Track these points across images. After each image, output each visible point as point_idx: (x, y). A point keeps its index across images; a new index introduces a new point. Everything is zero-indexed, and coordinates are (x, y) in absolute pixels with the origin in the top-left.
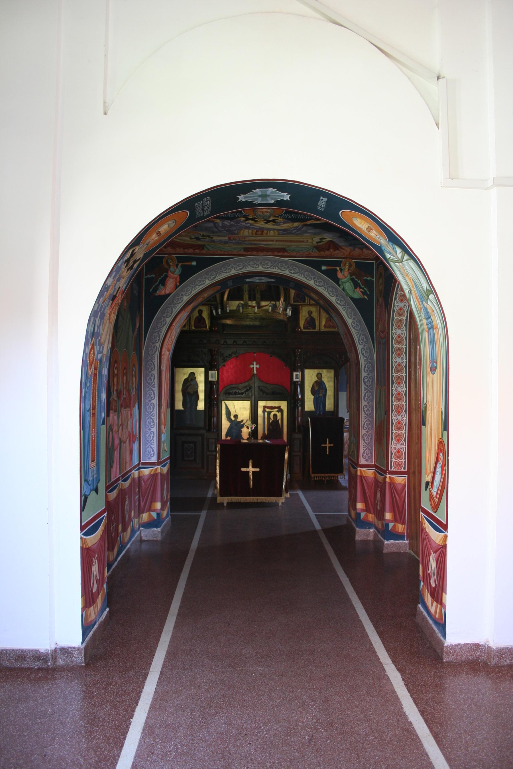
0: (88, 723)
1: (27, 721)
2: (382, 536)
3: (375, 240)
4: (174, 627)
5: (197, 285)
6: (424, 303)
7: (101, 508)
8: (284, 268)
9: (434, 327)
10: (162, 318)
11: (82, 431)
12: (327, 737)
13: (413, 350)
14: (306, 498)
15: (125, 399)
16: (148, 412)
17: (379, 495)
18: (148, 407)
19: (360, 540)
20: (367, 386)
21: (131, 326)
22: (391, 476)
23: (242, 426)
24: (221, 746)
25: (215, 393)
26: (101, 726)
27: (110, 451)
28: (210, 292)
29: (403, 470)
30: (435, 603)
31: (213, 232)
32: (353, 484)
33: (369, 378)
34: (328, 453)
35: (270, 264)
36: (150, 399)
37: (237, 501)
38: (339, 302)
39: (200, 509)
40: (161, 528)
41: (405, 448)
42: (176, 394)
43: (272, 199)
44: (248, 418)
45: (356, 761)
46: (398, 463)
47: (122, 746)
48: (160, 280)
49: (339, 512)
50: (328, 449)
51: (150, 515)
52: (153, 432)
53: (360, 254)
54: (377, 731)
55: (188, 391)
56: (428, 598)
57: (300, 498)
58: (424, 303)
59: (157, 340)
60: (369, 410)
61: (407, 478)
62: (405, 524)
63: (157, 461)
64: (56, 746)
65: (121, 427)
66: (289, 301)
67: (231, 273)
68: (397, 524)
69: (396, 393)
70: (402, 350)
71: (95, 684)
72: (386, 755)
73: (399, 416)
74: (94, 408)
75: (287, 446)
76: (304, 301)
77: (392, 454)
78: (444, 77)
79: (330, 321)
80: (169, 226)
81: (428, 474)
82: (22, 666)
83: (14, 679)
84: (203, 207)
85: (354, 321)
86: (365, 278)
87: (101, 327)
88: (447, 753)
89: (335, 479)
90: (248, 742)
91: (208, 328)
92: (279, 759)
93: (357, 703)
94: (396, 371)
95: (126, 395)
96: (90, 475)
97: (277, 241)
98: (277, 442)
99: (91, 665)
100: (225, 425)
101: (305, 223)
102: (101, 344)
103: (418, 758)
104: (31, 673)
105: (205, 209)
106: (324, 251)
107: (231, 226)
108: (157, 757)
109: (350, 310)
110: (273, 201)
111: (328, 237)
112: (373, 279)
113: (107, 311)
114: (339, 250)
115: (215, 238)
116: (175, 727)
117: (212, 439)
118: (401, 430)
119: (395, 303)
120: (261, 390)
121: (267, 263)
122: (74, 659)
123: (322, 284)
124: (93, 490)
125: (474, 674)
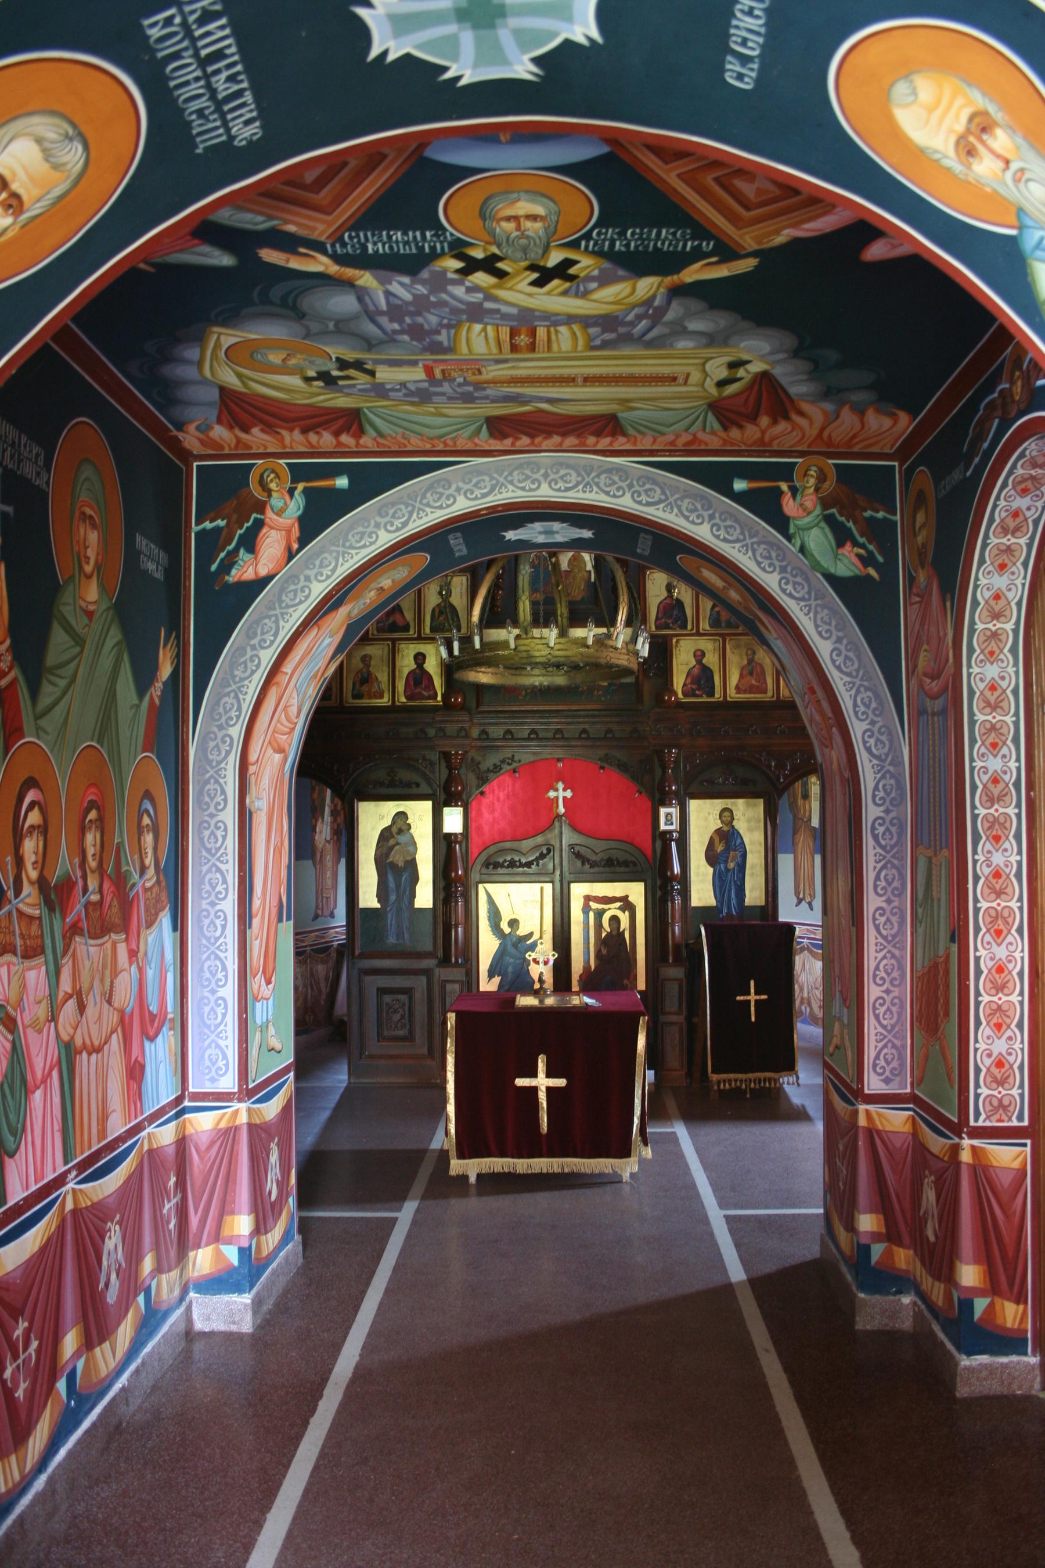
5: (352, 547)
8: (618, 489)
10: (249, 649)
16: (208, 939)
20: (883, 847)
22: (976, 1142)
29: (1015, 1123)
31: (370, 344)
32: (841, 1147)
33: (891, 822)
34: (753, 1019)
35: (574, 477)
36: (213, 897)
37: (506, 1170)
38: (789, 588)
39: (399, 1197)
41: (1022, 1050)
46: (1000, 1101)
49: (794, 1206)
50: (753, 1009)
51: (219, 1255)
53: (854, 436)
55: (390, 859)
57: (681, 1150)
59: (231, 718)
60: (892, 924)
61: (1028, 1149)
62: (1026, 1302)
63: (236, 1090)
68: (998, 1301)
69: (987, 871)
70: (1004, 730)
73: (999, 945)
75: (644, 1015)
77: (978, 1070)
79: (751, 674)
85: (838, 645)
86: (868, 514)
89: (773, 1085)
91: (439, 698)
94: (985, 798)
97: (588, 380)
98: (617, 1001)
100: (488, 946)
106: (741, 427)
114: (787, 418)
115: (384, 374)
118: (1006, 991)
120: (578, 855)
121: (566, 475)
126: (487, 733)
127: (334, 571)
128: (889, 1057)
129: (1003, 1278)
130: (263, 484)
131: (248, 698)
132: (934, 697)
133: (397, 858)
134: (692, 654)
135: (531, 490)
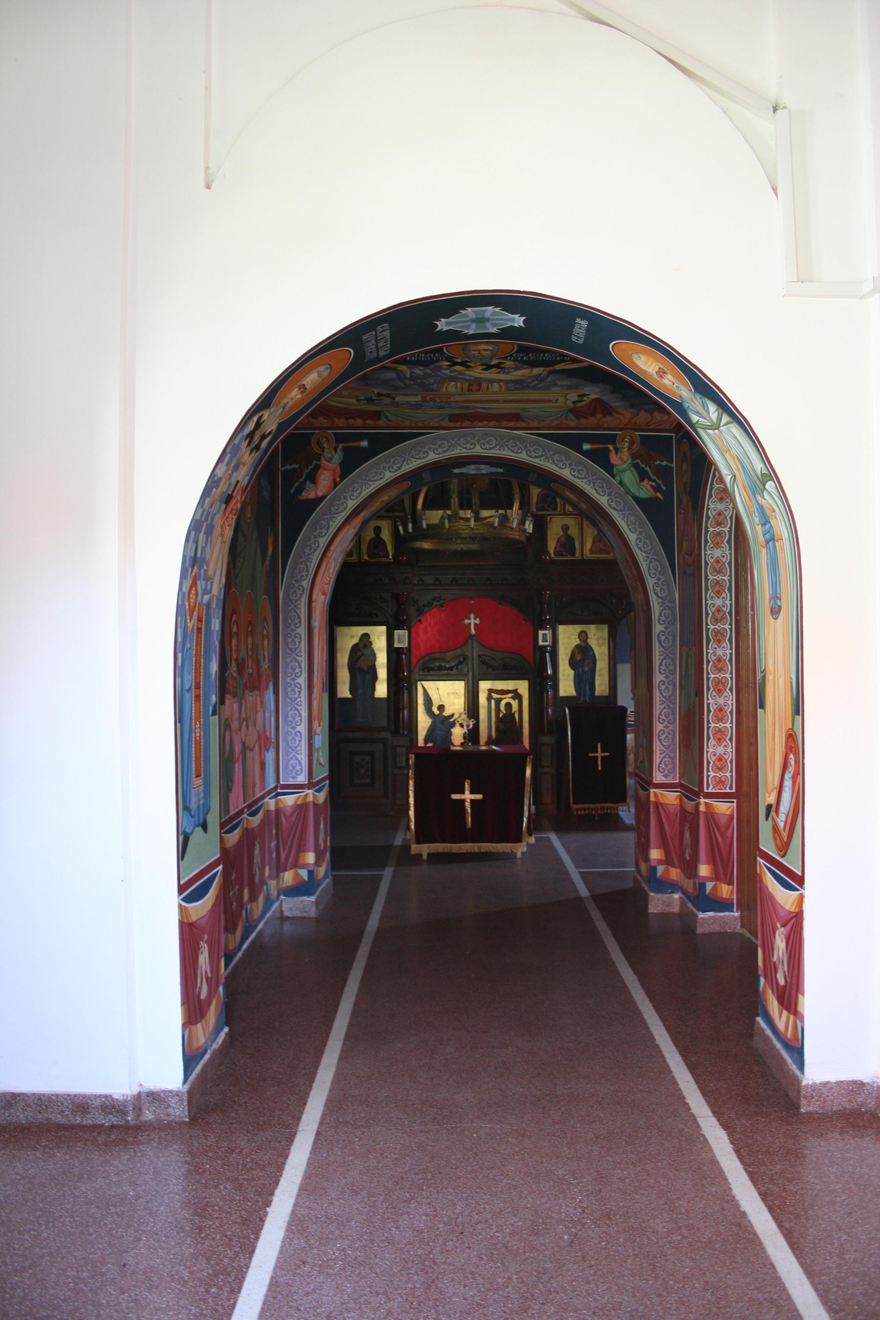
0: (196, 1213)
1: (94, 1210)
2: (693, 905)
3: (671, 390)
4: (340, 1058)
5: (370, 480)
6: (758, 497)
7: (212, 857)
9: (776, 538)
11: (178, 725)
12: (600, 1237)
13: (742, 585)
14: (563, 845)
15: (251, 675)
16: (290, 699)
17: (687, 834)
18: (290, 689)
19: (658, 913)
20: (664, 648)
21: (259, 550)
22: (707, 800)
23: (453, 725)
24: (420, 1252)
25: (405, 668)
26: (217, 1218)
27: (227, 762)
28: (393, 493)
29: (728, 791)
30: (785, 1013)
31: (396, 388)
32: (643, 817)
36: (293, 676)
37: (446, 851)
38: (613, 504)
39: (383, 866)
40: (316, 895)
41: (732, 752)
42: (338, 671)
43: (494, 325)
44: (462, 710)
45: (651, 1275)
46: (720, 779)
47: (253, 1251)
48: (307, 474)
50: (599, 762)
51: (297, 875)
52: (299, 732)
53: (648, 423)
54: (687, 1226)
55: (358, 665)
56: (773, 1004)
58: (759, 497)
59: (303, 576)
61: (735, 804)
62: (733, 885)
64: (143, 1251)
65: (245, 723)
66: (529, 509)
67: (428, 458)
68: (718, 883)
69: (714, 658)
70: (724, 584)
71: (207, 1152)
72: (702, 1266)
73: (720, 697)
74: (198, 687)
75: (529, 755)
76: (555, 509)
77: (708, 763)
78: (785, 108)
79: (600, 541)
80: (319, 376)
81: (769, 791)
82: (84, 1123)
83: (71, 1144)
84: (377, 341)
85: (640, 536)
86: (658, 463)
87: (208, 549)
88: (806, 1263)
89: (612, 812)
90: (466, 1245)
91: (391, 557)
92: (518, 1273)
93: (652, 1181)
94: (713, 620)
95: (252, 669)
96: (193, 800)
97: (505, 401)
98: (511, 749)
99: (200, 1120)
100: (424, 722)
101: (552, 368)
102: (207, 578)
103: (758, 1271)
104: (99, 1134)
105: (380, 344)
106: (586, 418)
107: (426, 376)
108: (312, 1268)
109: (632, 518)
110: (495, 329)
111: (593, 392)
112: (671, 465)
113: (218, 522)
114: (611, 414)
115: (399, 399)
116: (343, 1221)
117: (401, 746)
118: (723, 721)
119: (710, 503)
120: (484, 662)
121: (489, 441)
122: (170, 1110)
123: (584, 474)
124: (198, 826)
125: (854, 1132)
126: (423, 581)
127: (360, 493)
128: (667, 763)
129: (721, 872)
130: (319, 444)
131: (312, 565)
132: (690, 566)
133: (362, 664)
134: (560, 526)
135: (470, 449)
